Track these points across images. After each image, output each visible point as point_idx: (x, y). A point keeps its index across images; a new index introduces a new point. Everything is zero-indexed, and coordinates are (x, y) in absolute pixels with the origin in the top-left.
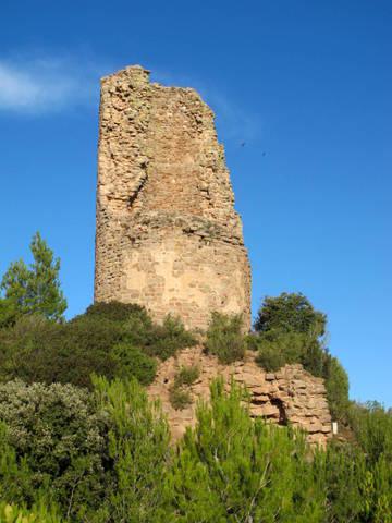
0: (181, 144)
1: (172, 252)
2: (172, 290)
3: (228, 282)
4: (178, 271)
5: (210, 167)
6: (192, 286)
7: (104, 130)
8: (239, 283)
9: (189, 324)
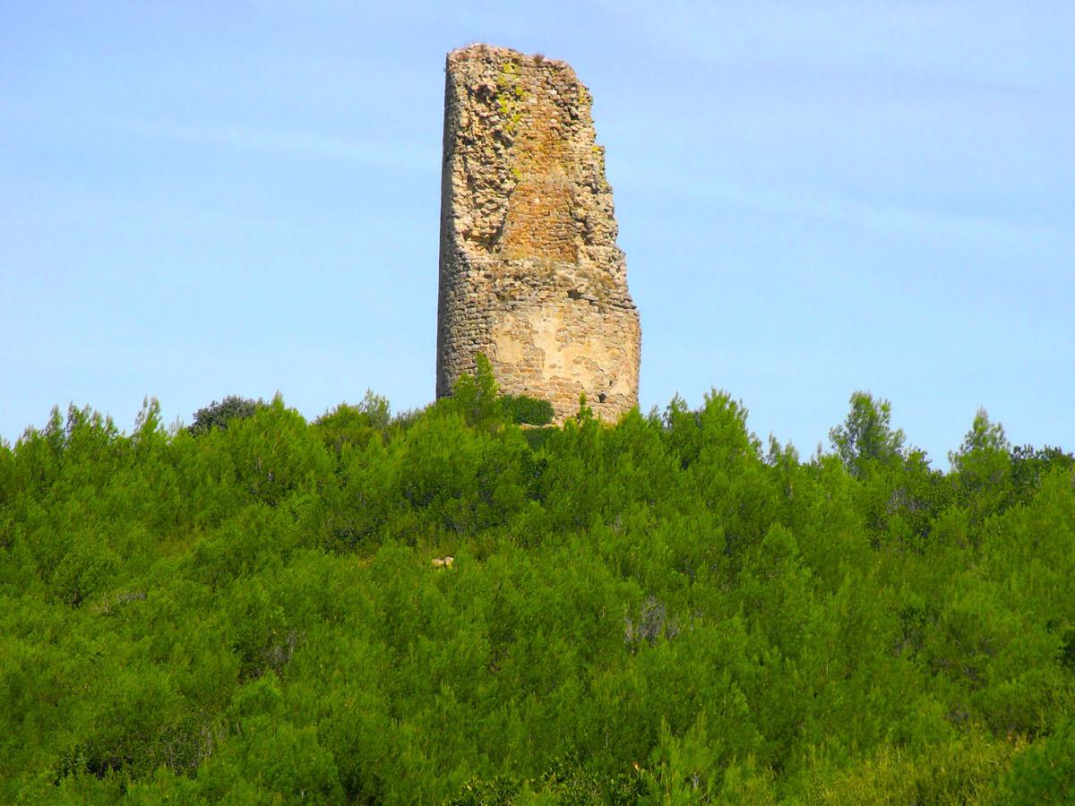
0: (549, 144)
1: (555, 320)
2: (553, 366)
3: (618, 358)
4: (564, 340)
5: (590, 185)
6: (577, 362)
7: (459, 142)
8: (629, 357)
9: (833, 787)
